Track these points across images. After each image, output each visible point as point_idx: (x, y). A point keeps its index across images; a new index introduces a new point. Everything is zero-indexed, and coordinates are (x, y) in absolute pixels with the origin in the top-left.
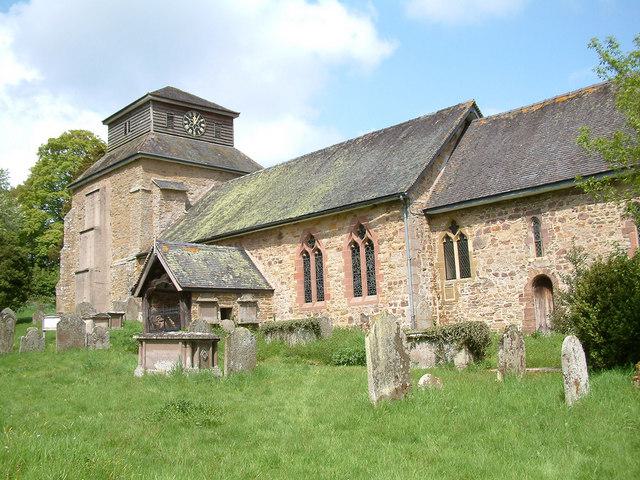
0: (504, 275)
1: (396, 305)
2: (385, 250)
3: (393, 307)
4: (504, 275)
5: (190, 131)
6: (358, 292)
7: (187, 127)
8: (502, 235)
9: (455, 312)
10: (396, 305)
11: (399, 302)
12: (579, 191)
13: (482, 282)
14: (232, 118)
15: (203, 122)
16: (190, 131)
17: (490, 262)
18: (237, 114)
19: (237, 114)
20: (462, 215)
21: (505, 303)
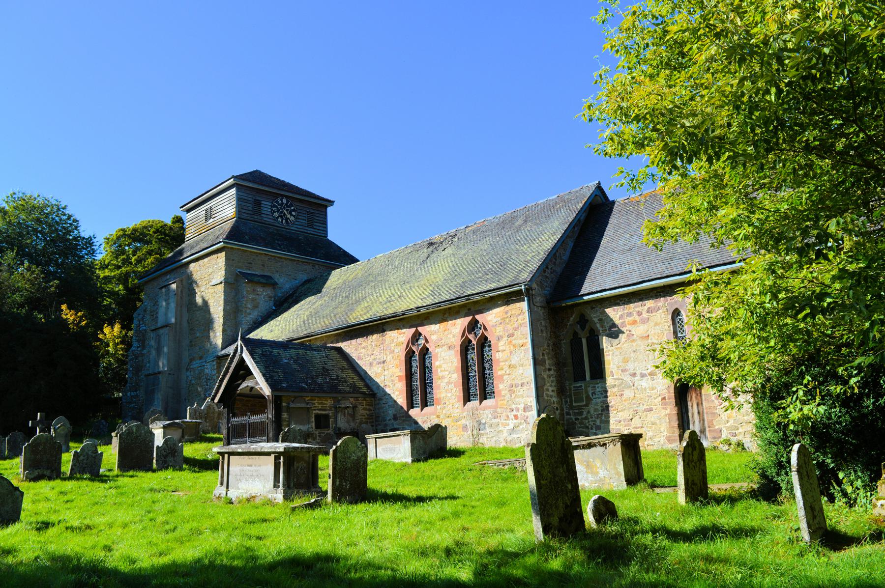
0: (643, 376)
1: (518, 410)
2: (504, 348)
3: (515, 413)
4: (643, 376)
5: (280, 219)
6: (467, 398)
7: (276, 214)
8: (536, 259)
9: (586, 418)
10: (518, 410)
11: (521, 406)
12: (814, 517)
13: (617, 383)
14: (326, 207)
15: (294, 210)
16: (280, 219)
17: (626, 361)
18: (331, 203)
19: (331, 203)
20: (592, 308)
21: (645, 407)
